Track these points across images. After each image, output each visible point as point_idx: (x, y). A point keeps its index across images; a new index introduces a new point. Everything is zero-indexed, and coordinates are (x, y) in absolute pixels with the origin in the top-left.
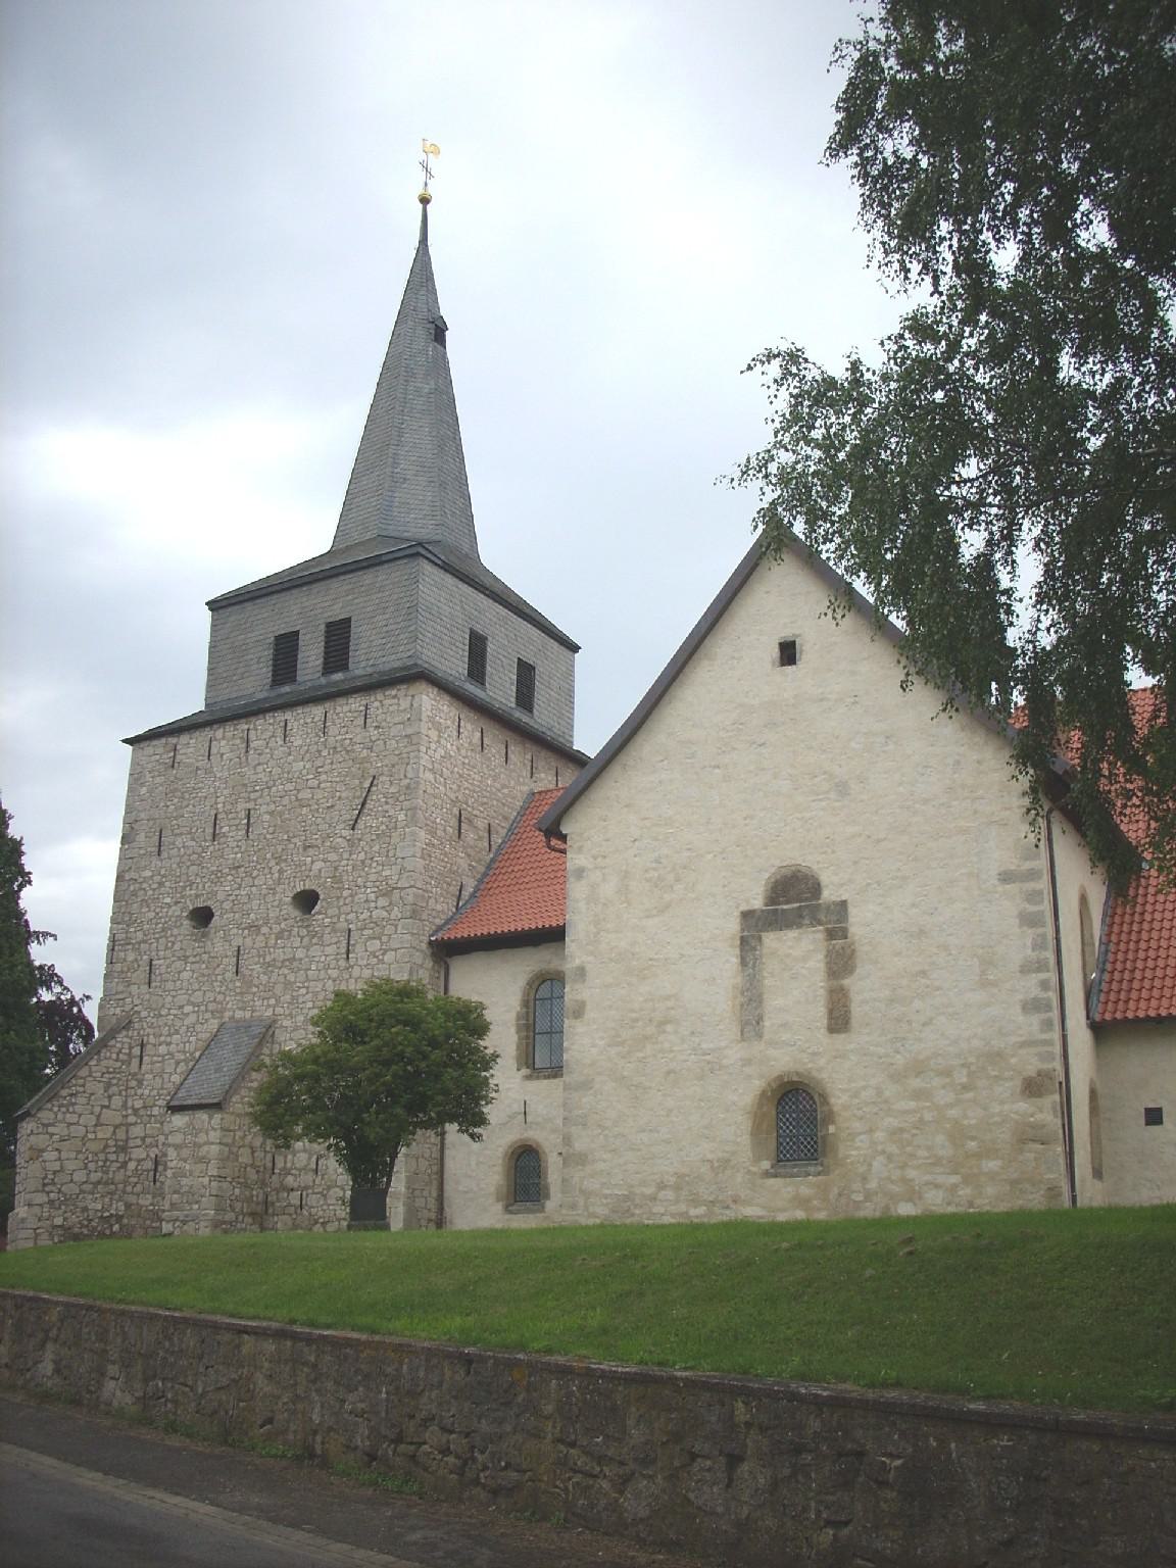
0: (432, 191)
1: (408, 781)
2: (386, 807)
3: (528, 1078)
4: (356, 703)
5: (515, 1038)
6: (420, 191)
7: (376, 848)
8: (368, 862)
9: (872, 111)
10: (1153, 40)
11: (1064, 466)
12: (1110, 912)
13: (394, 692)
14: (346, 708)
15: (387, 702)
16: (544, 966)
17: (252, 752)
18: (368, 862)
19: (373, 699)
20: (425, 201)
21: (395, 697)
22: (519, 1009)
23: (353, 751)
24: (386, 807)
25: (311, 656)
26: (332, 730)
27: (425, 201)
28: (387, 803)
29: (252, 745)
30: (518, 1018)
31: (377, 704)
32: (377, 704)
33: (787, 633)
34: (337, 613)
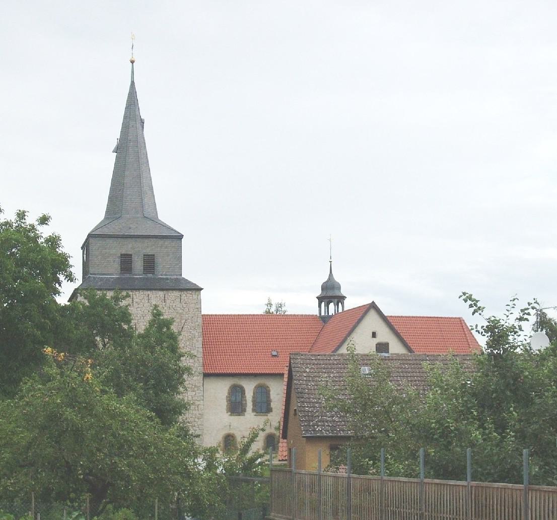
0: (135, 58)
2: (191, 331)
3: (231, 415)
4: (177, 293)
5: (226, 403)
6: (130, 58)
7: (188, 343)
8: (185, 347)
10: (547, 330)
13: (191, 292)
14: (172, 294)
15: (188, 295)
16: (236, 383)
17: (135, 303)
18: (185, 347)
20: (132, 62)
21: (191, 294)
22: (227, 395)
23: (177, 310)
24: (191, 331)
25: (138, 265)
27: (132, 62)
29: (134, 300)
31: (184, 295)
32: (184, 295)
33: (374, 330)
34: (149, 251)
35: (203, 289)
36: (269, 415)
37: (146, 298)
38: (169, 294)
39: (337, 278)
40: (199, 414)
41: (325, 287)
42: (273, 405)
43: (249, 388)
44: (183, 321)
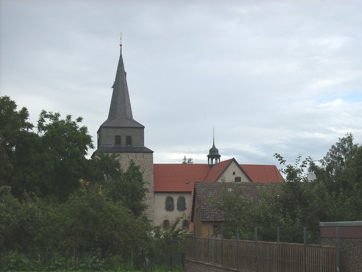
0: (122, 44)
1: (152, 168)
2: (148, 171)
4: (142, 154)
5: (165, 206)
8: (146, 179)
9: (330, 174)
11: (332, 165)
12: (275, 167)
14: (140, 154)
16: (169, 196)
17: (122, 158)
19: (144, 154)
20: (121, 45)
21: (148, 154)
24: (148, 171)
25: (124, 141)
26: (138, 158)
27: (121, 45)
28: (148, 171)
29: (122, 157)
30: (165, 203)
34: (129, 134)
35: (154, 152)
36: (185, 211)
37: (127, 156)
38: (138, 155)
39: (217, 147)
40: (152, 211)
41: (211, 151)
42: (186, 206)
43: (176, 198)
44: (145, 167)
